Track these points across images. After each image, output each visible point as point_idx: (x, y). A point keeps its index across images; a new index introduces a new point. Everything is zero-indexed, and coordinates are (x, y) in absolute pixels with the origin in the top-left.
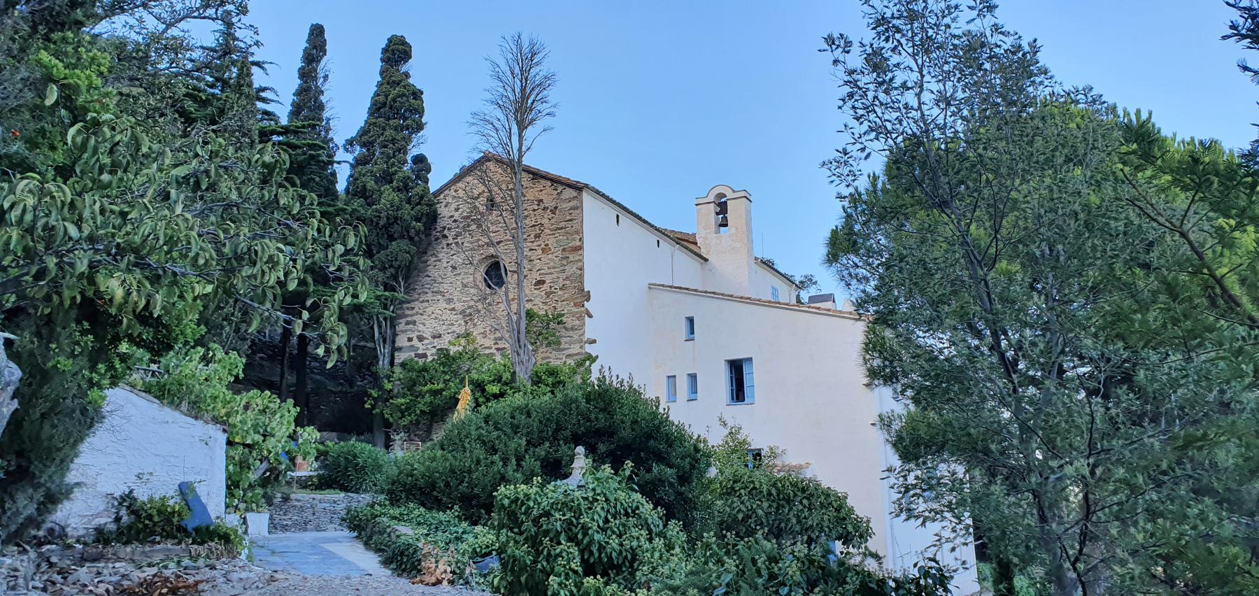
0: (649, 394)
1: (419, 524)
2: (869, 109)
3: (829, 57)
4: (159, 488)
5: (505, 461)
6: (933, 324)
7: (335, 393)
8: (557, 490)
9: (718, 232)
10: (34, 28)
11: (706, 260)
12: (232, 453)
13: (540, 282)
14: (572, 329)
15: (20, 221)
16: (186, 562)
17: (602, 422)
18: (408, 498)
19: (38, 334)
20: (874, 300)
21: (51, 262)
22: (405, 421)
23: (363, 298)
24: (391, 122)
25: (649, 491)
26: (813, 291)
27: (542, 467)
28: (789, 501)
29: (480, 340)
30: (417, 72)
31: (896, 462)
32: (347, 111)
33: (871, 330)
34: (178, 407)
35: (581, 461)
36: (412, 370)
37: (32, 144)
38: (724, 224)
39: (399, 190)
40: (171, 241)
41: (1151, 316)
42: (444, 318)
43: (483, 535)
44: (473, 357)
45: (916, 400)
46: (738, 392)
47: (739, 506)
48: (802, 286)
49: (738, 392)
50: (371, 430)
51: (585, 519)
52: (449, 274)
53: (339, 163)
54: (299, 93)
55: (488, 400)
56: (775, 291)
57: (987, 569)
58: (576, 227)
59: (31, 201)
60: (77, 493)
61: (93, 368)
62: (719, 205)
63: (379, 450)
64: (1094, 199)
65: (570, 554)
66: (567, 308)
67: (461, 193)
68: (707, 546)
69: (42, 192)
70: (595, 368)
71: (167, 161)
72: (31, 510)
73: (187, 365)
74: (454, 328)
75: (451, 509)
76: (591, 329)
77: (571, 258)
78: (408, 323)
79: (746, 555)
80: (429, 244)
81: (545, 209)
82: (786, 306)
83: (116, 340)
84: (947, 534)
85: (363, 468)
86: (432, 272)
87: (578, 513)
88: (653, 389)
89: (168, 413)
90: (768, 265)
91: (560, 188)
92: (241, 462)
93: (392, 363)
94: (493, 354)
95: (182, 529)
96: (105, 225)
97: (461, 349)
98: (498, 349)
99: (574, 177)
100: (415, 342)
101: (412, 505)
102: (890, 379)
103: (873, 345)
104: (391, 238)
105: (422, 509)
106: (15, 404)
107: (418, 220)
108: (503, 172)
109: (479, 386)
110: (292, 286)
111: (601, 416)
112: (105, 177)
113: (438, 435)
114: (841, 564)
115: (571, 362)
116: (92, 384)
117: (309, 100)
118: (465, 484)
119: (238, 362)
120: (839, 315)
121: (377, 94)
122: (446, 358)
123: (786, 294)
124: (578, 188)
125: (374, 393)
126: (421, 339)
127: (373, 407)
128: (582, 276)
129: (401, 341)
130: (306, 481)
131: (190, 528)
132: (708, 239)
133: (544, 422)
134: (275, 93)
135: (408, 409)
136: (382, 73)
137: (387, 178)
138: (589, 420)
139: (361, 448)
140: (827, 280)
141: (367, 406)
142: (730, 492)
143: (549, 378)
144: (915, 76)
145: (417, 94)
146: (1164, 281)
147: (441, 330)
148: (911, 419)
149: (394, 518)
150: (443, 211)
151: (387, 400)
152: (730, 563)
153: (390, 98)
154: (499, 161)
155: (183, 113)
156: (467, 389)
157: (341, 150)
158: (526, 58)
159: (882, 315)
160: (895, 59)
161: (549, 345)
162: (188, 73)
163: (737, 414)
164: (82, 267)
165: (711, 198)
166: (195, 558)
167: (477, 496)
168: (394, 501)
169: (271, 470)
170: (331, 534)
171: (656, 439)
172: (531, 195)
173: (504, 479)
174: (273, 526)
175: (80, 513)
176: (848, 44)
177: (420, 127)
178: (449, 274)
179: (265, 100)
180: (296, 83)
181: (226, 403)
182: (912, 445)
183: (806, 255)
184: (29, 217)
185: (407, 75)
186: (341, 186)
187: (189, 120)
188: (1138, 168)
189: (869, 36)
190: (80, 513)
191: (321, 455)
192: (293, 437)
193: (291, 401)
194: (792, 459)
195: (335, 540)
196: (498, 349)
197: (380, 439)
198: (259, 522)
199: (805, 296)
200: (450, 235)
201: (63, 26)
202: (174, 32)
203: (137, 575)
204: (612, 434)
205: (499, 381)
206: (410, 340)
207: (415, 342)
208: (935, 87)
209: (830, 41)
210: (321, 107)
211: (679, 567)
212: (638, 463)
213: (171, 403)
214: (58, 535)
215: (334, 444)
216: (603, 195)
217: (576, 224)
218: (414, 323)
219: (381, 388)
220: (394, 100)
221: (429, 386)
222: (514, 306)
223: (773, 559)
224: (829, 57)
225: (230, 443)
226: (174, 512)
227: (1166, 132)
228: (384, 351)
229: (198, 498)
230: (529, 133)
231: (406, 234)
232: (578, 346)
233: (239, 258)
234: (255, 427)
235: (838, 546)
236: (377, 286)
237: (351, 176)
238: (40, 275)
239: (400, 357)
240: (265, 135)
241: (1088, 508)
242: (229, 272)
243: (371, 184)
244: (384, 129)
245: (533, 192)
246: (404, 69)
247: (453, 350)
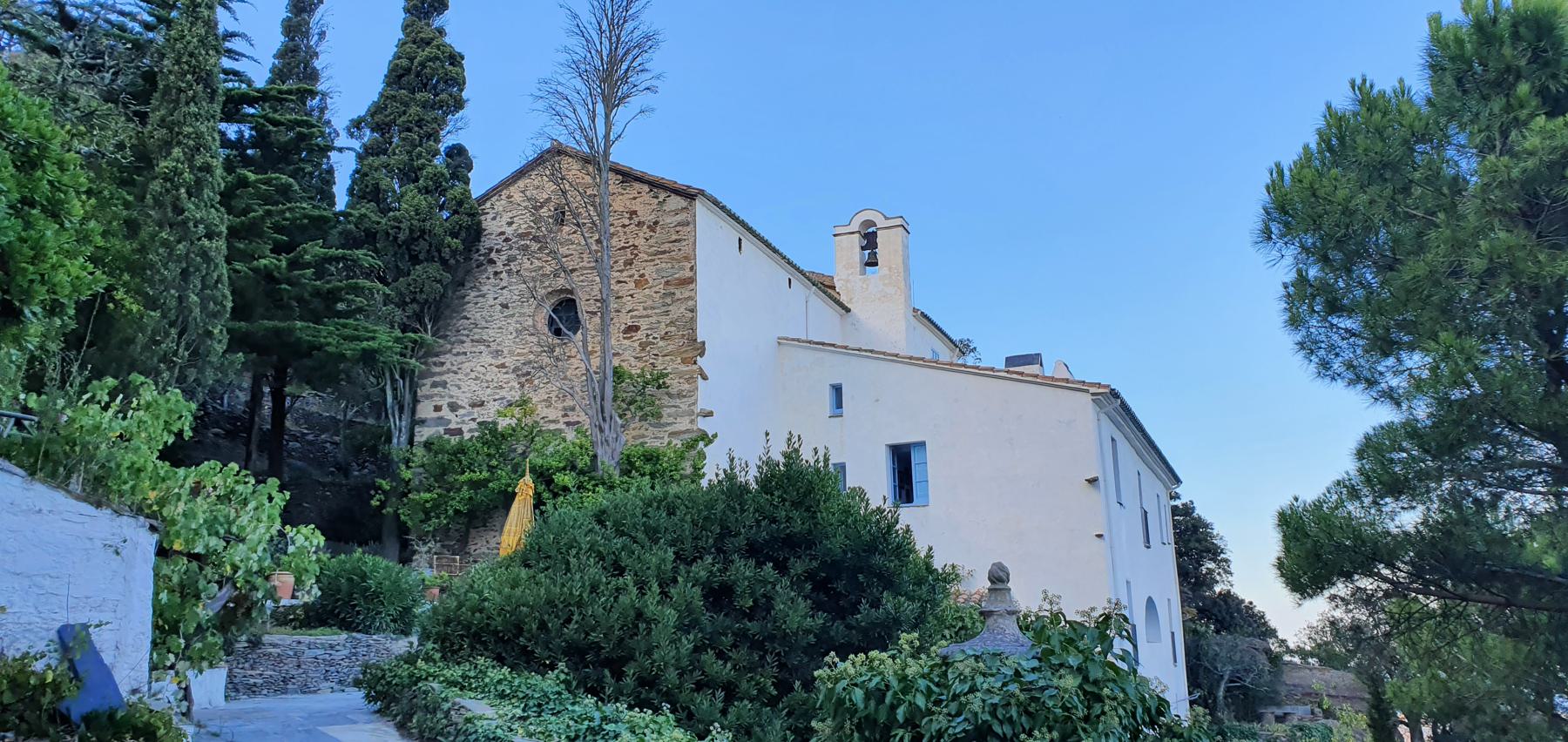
1: (502, 696)
7: (324, 485)
9: (863, 273)
11: (848, 310)
12: (165, 570)
13: (632, 329)
14: (680, 395)
18: (473, 648)
24: (418, 96)
27: (705, 597)
29: (542, 411)
32: (352, 81)
34: (63, 485)
36: (442, 451)
38: (872, 263)
39: (427, 192)
42: (485, 378)
44: (532, 434)
50: (378, 538)
52: (497, 315)
53: (340, 150)
54: (281, 55)
55: (556, 495)
58: (686, 249)
62: (866, 236)
66: (672, 365)
67: (518, 197)
74: (503, 393)
75: (552, 667)
76: (705, 395)
77: (678, 295)
78: (435, 385)
80: (468, 272)
81: (640, 224)
85: (376, 595)
86: (473, 312)
89: (42, 495)
91: (662, 196)
92: (182, 586)
93: (411, 442)
94: (561, 431)
97: (514, 422)
98: (568, 424)
99: (682, 179)
100: (446, 413)
101: (481, 660)
104: (415, 260)
105: (590, 700)
107: (455, 235)
108: (581, 169)
109: (544, 477)
111: (795, 514)
115: (677, 442)
117: (297, 61)
118: (573, 626)
121: (397, 57)
122: (493, 437)
123: (946, 354)
124: (689, 195)
125: (386, 485)
126: (454, 407)
127: (383, 504)
128: (693, 320)
129: (425, 410)
130: (286, 614)
131: (75, 715)
133: (702, 524)
134: (249, 40)
135: (436, 506)
136: (405, 28)
138: (774, 521)
139: (377, 565)
141: (375, 503)
145: (455, 59)
147: (484, 395)
149: (452, 683)
150: (491, 225)
151: (405, 495)
153: (416, 62)
156: (528, 478)
157: (343, 134)
161: (643, 418)
165: (855, 226)
167: (597, 647)
168: (450, 652)
169: (239, 600)
171: (883, 553)
172: (619, 204)
174: (234, 688)
177: (459, 104)
178: (497, 315)
179: (231, 53)
180: (277, 40)
181: (157, 480)
185: (441, 32)
193: (273, 482)
196: (568, 424)
197: (393, 546)
198: (209, 685)
200: (500, 260)
204: (810, 544)
205: (573, 468)
206: (438, 408)
207: (446, 413)
210: (313, 76)
213: (53, 475)
216: (723, 208)
217: (685, 248)
218: (444, 384)
219: (394, 476)
220: (423, 65)
221: (467, 476)
222: (595, 362)
225: (163, 552)
226: (43, 684)
229: (95, 654)
230: (621, 114)
231: (435, 253)
232: (687, 420)
234: (211, 526)
236: (392, 327)
237: (357, 171)
239: (423, 434)
244: (407, 105)
245: (622, 199)
246: (438, 22)
247: (503, 424)
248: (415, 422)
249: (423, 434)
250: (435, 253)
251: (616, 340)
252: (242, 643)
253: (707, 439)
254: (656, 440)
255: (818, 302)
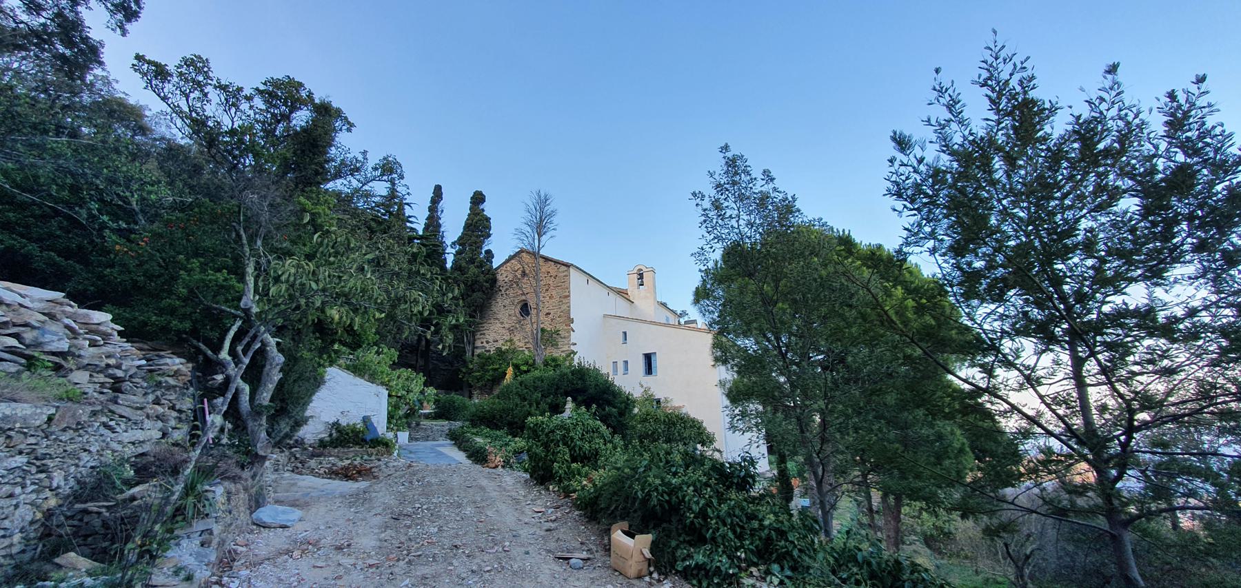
0: (604, 371)
2: (714, 228)
3: (694, 202)
4: (352, 419)
5: (531, 405)
6: (746, 335)
8: (558, 419)
10: (297, 186)
13: (548, 314)
15: (287, 281)
16: (366, 457)
17: (580, 384)
19: (293, 339)
20: (717, 323)
21: (303, 301)
22: (480, 384)
23: (461, 320)
25: (604, 420)
26: (686, 319)
28: (674, 424)
29: (518, 343)
30: (488, 209)
31: (727, 402)
32: (452, 227)
33: (715, 338)
34: (362, 376)
35: (570, 405)
37: (294, 242)
40: (364, 291)
41: (854, 330)
42: (499, 332)
43: (520, 442)
44: (514, 351)
45: (739, 373)
46: (649, 369)
47: (650, 427)
48: (681, 316)
49: (649, 369)
51: (572, 434)
56: (667, 319)
57: (773, 458)
59: (293, 271)
60: (310, 422)
61: (320, 357)
63: (466, 400)
64: (824, 273)
65: (564, 452)
66: (561, 327)
68: (634, 447)
69: (298, 266)
70: (576, 358)
71: (362, 253)
72: (288, 429)
73: (369, 356)
76: (574, 337)
79: (654, 450)
82: (673, 326)
83: (333, 342)
84: (754, 439)
86: (494, 309)
87: (568, 430)
88: (605, 369)
89: (359, 380)
90: (664, 305)
95: (364, 440)
96: (330, 282)
99: (565, 260)
102: (725, 362)
103: (717, 345)
104: (473, 291)
106: (281, 375)
108: (530, 259)
109: (516, 367)
110: (426, 314)
112: (332, 259)
113: (496, 392)
114: (701, 455)
116: (320, 365)
117: (433, 222)
119: (395, 354)
120: (699, 330)
123: (673, 320)
124: (568, 266)
129: (478, 344)
132: (634, 292)
137: (472, 261)
139: (457, 398)
140: (694, 313)
142: (644, 420)
143: (553, 363)
144: (736, 212)
145: (488, 219)
146: (860, 312)
147: (498, 338)
148: (735, 382)
150: (499, 277)
152: (646, 455)
154: (528, 253)
155: (369, 228)
158: (543, 202)
159: (721, 329)
160: (726, 204)
162: (372, 208)
163: (649, 381)
164: (318, 304)
166: (370, 455)
168: (474, 425)
170: (441, 442)
173: (530, 414)
174: (411, 439)
175: (311, 432)
176: (703, 196)
177: (489, 236)
182: (736, 395)
183: (683, 300)
184: (292, 279)
186: (449, 265)
187: (373, 232)
188: (846, 258)
189: (713, 192)
190: (311, 432)
191: (437, 402)
192: (422, 392)
194: (676, 403)
195: (443, 446)
197: (467, 394)
198: (403, 436)
199: (682, 321)
201: (311, 184)
202: (366, 187)
203: (340, 464)
208: (746, 218)
209: (694, 194)
210: (440, 226)
211: (620, 458)
212: (599, 406)
214: (300, 443)
215: (443, 396)
223: (668, 453)
224: (694, 202)
225: (389, 396)
227: (858, 241)
228: (468, 348)
229: (372, 424)
230: (544, 238)
231: (481, 289)
233: (399, 300)
234: (403, 387)
235: (699, 446)
238: (298, 307)
239: (478, 351)
240: (411, 239)
241: (824, 423)
242: (394, 307)
243: (464, 264)
245: (545, 267)
248: (474, 348)
249: (478, 351)
250: (481, 289)
251: (542, 317)
252: (414, 425)
253: (575, 353)
254: (556, 353)
255: (621, 301)
